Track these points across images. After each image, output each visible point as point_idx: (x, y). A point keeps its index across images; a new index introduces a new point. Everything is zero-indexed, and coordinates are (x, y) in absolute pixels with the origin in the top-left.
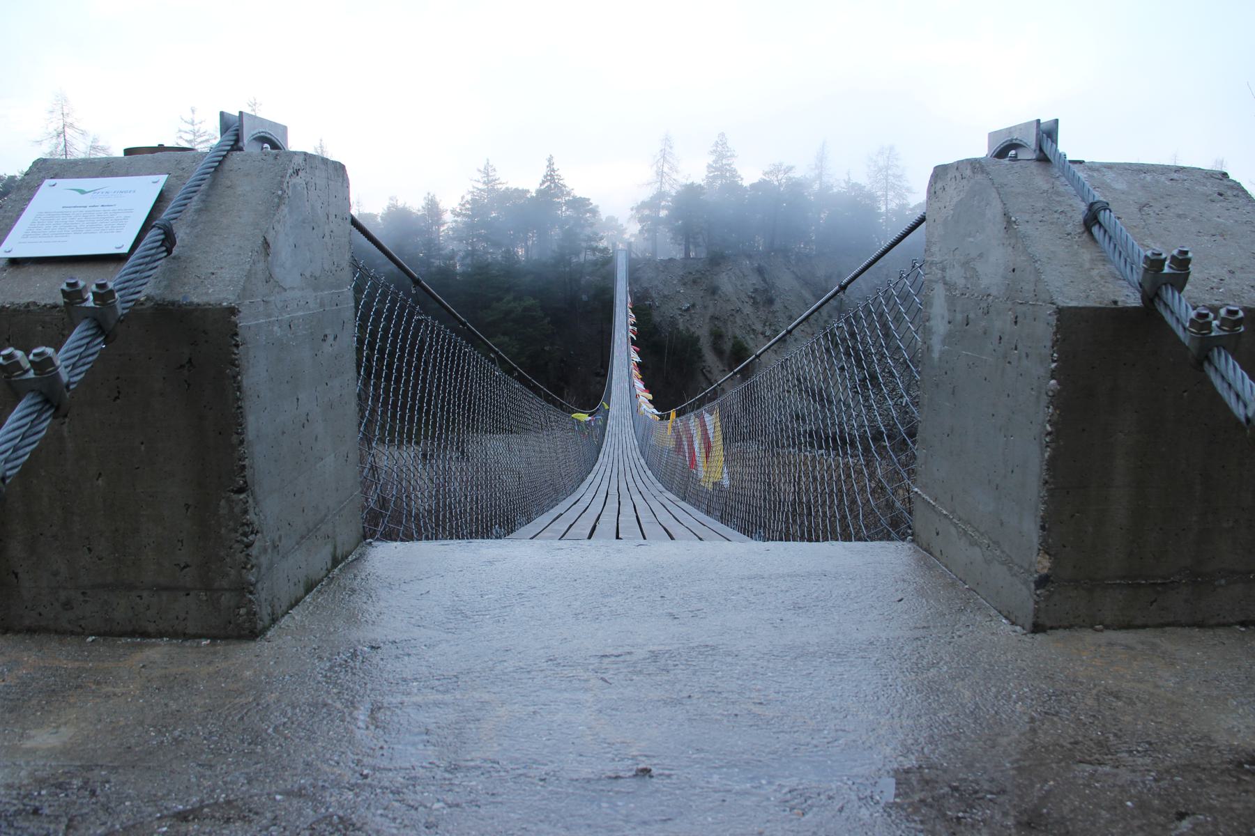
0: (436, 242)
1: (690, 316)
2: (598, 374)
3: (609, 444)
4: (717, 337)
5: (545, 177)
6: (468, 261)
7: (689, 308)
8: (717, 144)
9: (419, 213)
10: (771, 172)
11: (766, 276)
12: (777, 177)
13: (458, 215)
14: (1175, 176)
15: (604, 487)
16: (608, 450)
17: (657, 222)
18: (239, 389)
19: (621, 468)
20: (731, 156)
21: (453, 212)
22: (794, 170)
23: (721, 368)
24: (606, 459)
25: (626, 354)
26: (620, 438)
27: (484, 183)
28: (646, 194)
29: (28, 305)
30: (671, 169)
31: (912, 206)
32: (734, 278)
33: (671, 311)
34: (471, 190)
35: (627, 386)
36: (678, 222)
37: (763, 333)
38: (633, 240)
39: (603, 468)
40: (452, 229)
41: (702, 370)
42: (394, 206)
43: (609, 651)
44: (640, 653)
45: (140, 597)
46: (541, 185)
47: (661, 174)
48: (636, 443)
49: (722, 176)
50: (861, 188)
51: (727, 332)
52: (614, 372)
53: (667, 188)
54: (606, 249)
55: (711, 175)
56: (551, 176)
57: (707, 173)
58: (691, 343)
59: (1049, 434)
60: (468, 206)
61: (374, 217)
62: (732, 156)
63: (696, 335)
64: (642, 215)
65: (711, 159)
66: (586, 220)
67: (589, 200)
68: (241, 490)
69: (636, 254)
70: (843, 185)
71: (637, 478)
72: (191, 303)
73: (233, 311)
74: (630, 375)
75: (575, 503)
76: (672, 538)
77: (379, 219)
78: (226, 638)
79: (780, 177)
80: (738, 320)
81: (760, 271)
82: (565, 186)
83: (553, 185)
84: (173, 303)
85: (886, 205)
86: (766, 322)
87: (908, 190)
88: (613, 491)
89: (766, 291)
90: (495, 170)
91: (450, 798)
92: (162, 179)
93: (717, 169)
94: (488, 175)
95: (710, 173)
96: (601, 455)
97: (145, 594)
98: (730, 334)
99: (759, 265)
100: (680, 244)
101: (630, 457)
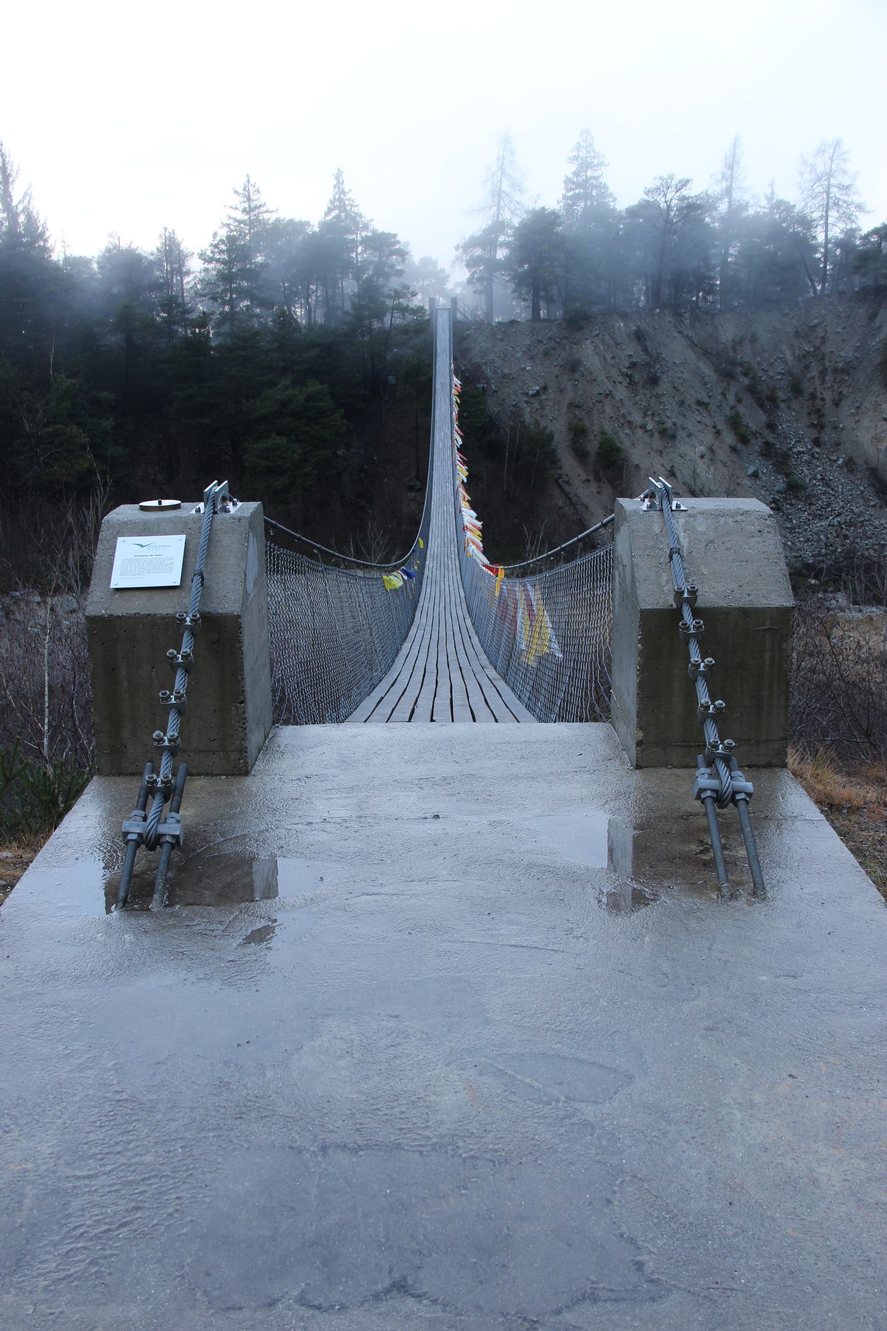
0: (180, 300)
1: (540, 403)
2: (411, 489)
3: (428, 596)
4: (578, 432)
5: (332, 202)
6: (226, 328)
7: (538, 391)
8: (578, 147)
9: (152, 258)
10: (657, 189)
11: (648, 344)
12: (665, 195)
13: (210, 260)
14: (739, 518)
15: (421, 663)
16: (426, 606)
17: (492, 266)
18: (242, 653)
19: (442, 633)
20: (599, 165)
21: (202, 256)
22: (689, 186)
23: (584, 477)
24: (424, 620)
25: (450, 463)
26: (442, 588)
27: (244, 210)
28: (476, 226)
29: (135, 614)
30: (512, 185)
31: (864, 232)
32: (602, 348)
33: (513, 396)
34: (226, 221)
35: (452, 510)
36: (522, 266)
37: (643, 427)
38: (458, 291)
39: (421, 632)
40: (202, 281)
41: (557, 480)
42: (117, 247)
43: (423, 777)
44: (437, 778)
45: (189, 756)
46: (326, 214)
47: (498, 194)
48: (462, 594)
49: (586, 196)
50: (789, 208)
51: (592, 425)
52: (435, 490)
53: (506, 215)
54: (420, 309)
55: (570, 194)
56: (340, 200)
57: (564, 192)
58: (544, 440)
59: (639, 670)
60: (223, 247)
61: (83, 263)
62: (600, 165)
63: (548, 431)
64: (472, 257)
65: (570, 170)
66: (392, 267)
67: (395, 236)
68: (242, 702)
69: (464, 315)
70: (764, 202)
71: (460, 648)
72: (218, 613)
73: (239, 617)
74: (456, 494)
75: (393, 685)
76: (497, 721)
77: (95, 266)
78: (233, 775)
79: (669, 197)
80: (607, 408)
81: (639, 336)
82: (360, 216)
83: (343, 215)
84: (209, 613)
85: (826, 232)
86: (647, 410)
87: (860, 208)
88: (431, 668)
89: (648, 365)
90: (259, 192)
91: (361, 825)
92: (184, 537)
93: (578, 185)
94: (249, 199)
95: (568, 190)
96: (418, 614)
97: (192, 754)
98: (596, 428)
99: (638, 327)
100: (525, 300)
101: (454, 615)
